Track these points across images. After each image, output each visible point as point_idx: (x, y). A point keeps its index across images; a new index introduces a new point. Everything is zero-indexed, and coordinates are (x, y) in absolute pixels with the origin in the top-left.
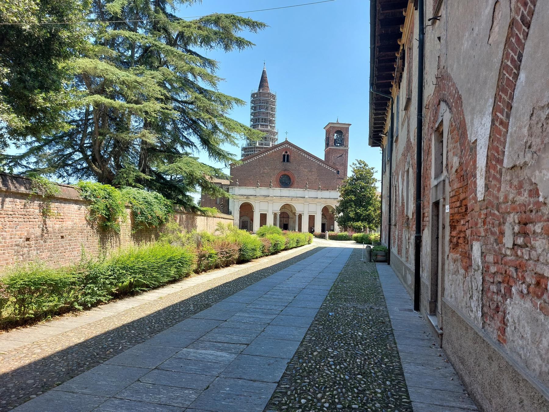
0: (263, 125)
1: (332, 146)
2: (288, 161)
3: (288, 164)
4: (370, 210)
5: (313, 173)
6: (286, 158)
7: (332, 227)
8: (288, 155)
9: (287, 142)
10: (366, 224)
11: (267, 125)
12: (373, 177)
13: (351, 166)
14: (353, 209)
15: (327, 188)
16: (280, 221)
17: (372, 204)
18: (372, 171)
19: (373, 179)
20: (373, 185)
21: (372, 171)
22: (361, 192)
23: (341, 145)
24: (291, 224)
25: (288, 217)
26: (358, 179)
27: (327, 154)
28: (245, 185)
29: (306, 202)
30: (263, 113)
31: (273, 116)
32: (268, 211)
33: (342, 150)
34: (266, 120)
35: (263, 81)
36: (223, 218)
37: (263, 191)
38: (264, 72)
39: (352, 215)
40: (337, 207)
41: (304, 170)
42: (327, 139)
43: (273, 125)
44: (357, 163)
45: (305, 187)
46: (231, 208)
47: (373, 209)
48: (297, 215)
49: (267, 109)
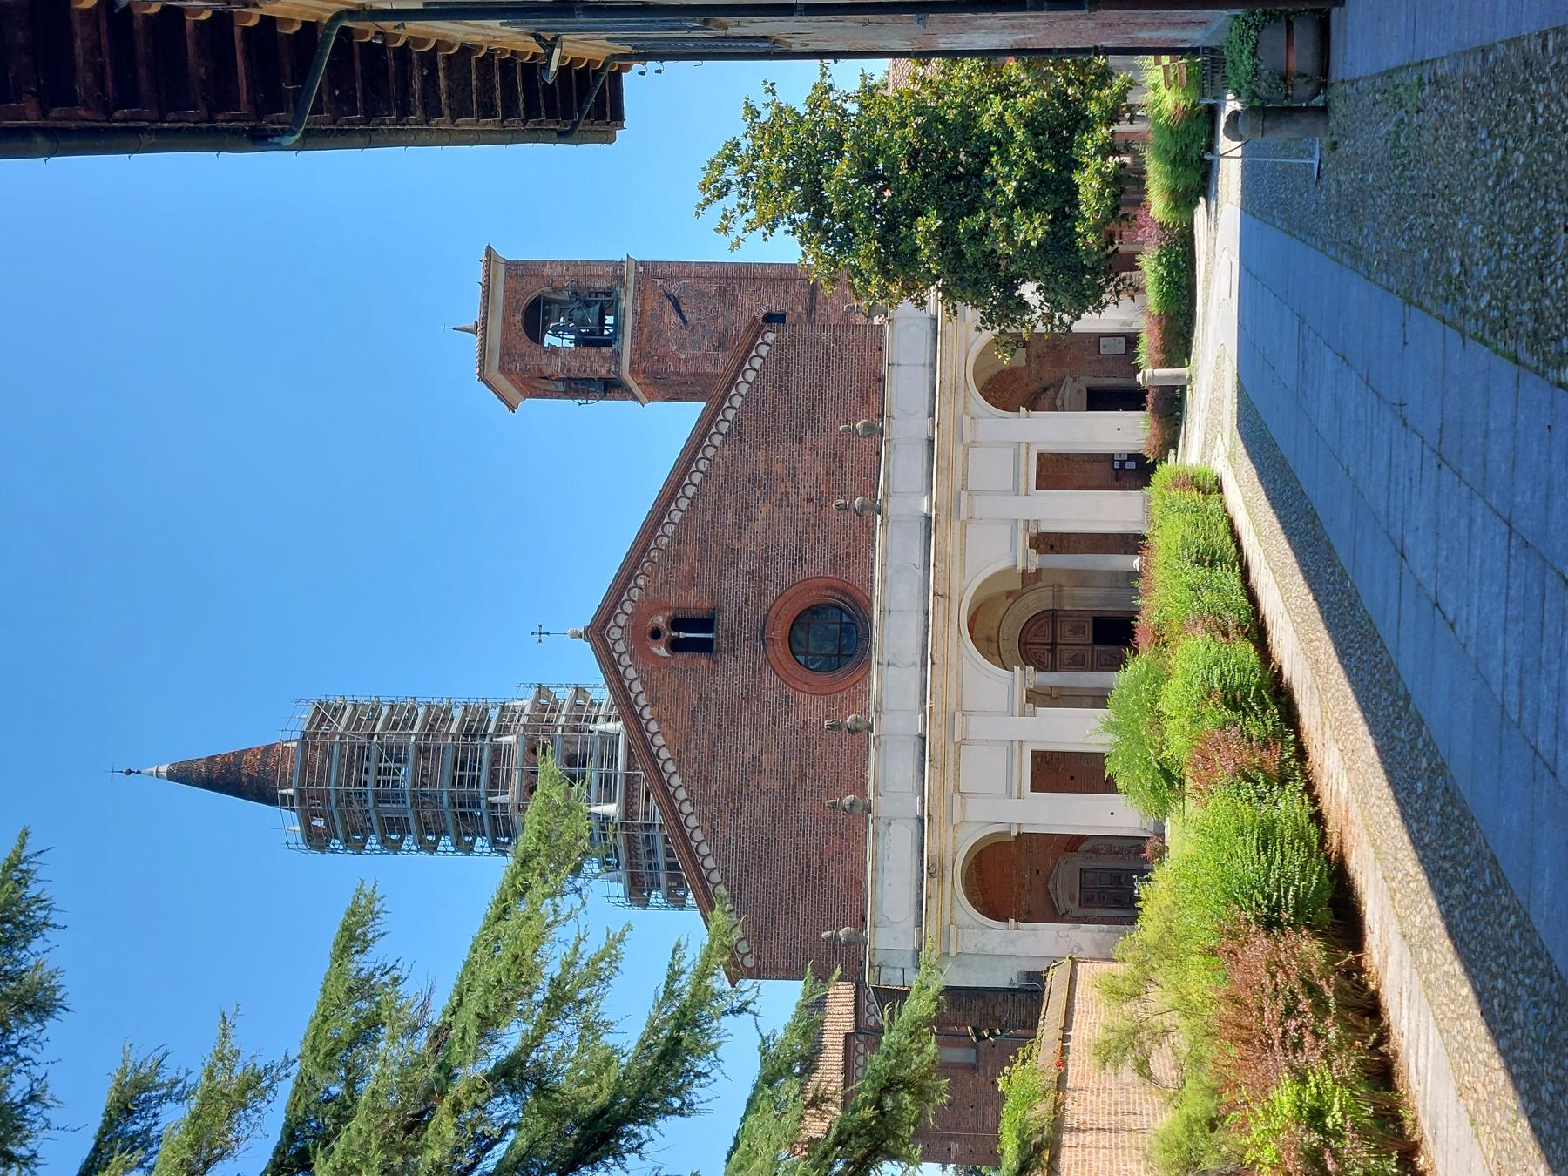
1: (617, 357)
2: (707, 624)
3: (724, 619)
4: (1000, 121)
5: (779, 469)
6: (693, 634)
7: (1107, 347)
8: (669, 623)
9: (596, 633)
11: (496, 750)
12: (803, 110)
13: (737, 244)
14: (996, 223)
15: (872, 384)
16: (1078, 664)
17: (964, 110)
19: (815, 105)
22: (889, 178)
23: (607, 302)
24: (1093, 600)
25: (1052, 616)
26: (814, 199)
30: (421, 776)
31: (437, 718)
33: (641, 296)
34: (465, 763)
36: (1067, 1025)
37: (891, 775)
38: (182, 775)
39: (1033, 229)
40: (987, 320)
41: (758, 526)
42: (578, 386)
44: (718, 206)
46: (1002, 977)
47: (997, 104)
48: (1035, 561)
49: (396, 754)
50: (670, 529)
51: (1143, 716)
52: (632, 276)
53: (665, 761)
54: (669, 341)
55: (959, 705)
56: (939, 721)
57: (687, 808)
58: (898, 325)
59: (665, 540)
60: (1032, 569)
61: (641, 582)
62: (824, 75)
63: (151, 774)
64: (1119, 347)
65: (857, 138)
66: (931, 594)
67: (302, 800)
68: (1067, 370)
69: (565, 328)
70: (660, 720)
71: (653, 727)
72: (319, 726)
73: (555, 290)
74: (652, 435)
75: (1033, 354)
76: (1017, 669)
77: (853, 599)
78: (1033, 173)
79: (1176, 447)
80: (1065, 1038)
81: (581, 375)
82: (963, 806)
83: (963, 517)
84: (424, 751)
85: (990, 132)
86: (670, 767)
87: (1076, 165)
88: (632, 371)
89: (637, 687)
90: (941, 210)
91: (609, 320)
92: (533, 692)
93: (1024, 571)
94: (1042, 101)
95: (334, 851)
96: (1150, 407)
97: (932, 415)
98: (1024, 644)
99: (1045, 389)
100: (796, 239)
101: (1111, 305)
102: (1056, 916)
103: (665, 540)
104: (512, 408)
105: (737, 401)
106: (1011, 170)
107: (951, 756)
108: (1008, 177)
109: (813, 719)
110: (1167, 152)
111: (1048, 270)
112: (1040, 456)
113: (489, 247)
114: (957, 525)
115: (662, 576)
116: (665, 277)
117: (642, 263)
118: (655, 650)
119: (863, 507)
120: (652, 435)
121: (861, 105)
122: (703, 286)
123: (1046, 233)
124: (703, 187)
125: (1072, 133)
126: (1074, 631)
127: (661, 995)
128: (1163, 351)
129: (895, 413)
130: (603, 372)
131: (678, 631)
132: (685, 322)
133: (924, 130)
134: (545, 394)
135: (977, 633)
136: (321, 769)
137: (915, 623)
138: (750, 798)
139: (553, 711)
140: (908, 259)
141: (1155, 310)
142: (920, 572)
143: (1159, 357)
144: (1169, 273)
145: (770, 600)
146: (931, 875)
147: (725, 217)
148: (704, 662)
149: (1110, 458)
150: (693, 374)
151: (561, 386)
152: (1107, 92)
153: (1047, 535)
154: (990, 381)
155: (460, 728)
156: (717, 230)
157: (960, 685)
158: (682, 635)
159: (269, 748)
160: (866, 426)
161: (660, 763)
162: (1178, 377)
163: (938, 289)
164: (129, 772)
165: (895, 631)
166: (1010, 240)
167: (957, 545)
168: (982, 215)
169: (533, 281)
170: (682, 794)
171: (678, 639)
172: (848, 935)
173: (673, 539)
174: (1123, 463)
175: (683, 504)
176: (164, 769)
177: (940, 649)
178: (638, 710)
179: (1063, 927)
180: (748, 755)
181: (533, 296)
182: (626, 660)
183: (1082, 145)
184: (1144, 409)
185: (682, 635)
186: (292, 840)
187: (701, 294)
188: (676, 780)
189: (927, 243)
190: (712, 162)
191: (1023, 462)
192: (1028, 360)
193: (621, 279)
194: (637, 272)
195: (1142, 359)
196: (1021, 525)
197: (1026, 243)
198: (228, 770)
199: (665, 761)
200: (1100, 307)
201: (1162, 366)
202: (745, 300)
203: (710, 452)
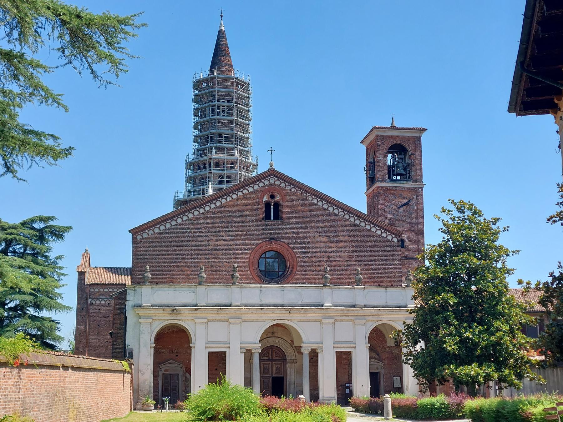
0: (223, 149)
1: (384, 181)
3: (279, 224)
4: (498, 330)
5: (341, 244)
6: (273, 211)
7: (397, 380)
8: (279, 203)
10: (491, 370)
11: (233, 149)
12: (497, 243)
13: (437, 217)
14: (452, 328)
15: (378, 280)
16: (263, 371)
17: (502, 314)
18: (494, 227)
19: (500, 248)
20: (499, 265)
21: (494, 227)
22: (469, 283)
23: (406, 177)
24: (291, 378)
25: (283, 359)
26: (460, 249)
27: (373, 201)
28: (171, 280)
29: (326, 316)
30: (222, 122)
31: (244, 128)
32: (228, 344)
33: (409, 190)
34: (228, 138)
35: (220, 55)
36: (74, 368)
37: (216, 293)
38: (221, 35)
39: (451, 345)
40: (408, 327)
41: (317, 237)
42: (371, 167)
43: (247, 149)
44: (453, 208)
45: (321, 280)
46: (130, 342)
47: (506, 328)
48: (306, 351)
49: (230, 113)
50: (315, 201)
51: (231, 401)
52: (417, 186)
53: (221, 201)
54: (391, 202)
55: (245, 320)
56: (238, 312)
57: (202, 211)
58: (403, 292)
59: (310, 199)
60: (302, 350)
61: (293, 190)
62: (513, 252)
63: (221, 24)
64: (397, 385)
65: (487, 267)
66: (290, 308)
67: (212, 78)
68: (386, 363)
69: (395, 161)
70: (238, 198)
71: (234, 196)
72: (240, 84)
73: (410, 156)
74: (354, 194)
75: (392, 349)
76: (260, 345)
77: (288, 276)
78: (476, 345)
79: (355, 411)
80: (65, 368)
81: (376, 167)
82: (202, 323)
83: (324, 320)
84: (231, 123)
85: (493, 326)
86: (218, 204)
87: (480, 366)
88: (379, 187)
89: (251, 189)
90: (457, 304)
91: (399, 178)
92: (254, 163)
93: (301, 347)
94: (507, 348)
95: (194, 92)
96: (373, 399)
97: (366, 306)
98: (272, 348)
99: (378, 355)
100: (441, 242)
101: (417, 381)
102: (157, 364)
103: (310, 199)
104: (362, 142)
105: (368, 227)
106: (477, 335)
107: (223, 318)
108: (473, 334)
109: (239, 261)
110: (504, 408)
111: (433, 352)
112: (350, 353)
113: (426, 130)
114: (319, 318)
115: (295, 198)
116: (417, 199)
117: (422, 190)
118: (266, 196)
119: (326, 278)
120: (354, 194)
121: (501, 268)
122: (414, 214)
123: (450, 351)
124: (462, 202)
125: (493, 362)
126: (278, 369)
127: (26, 128)
128: (399, 406)
129: (366, 291)
130: (378, 176)
131: (274, 206)
132: (399, 208)
133: (492, 296)
134: (368, 155)
135: (275, 328)
136: (224, 85)
137: (280, 301)
138: (206, 236)
139: (247, 170)
140: (435, 291)
141: (419, 402)
142: (300, 303)
143: (396, 404)
144: (436, 409)
145: (287, 242)
146: (173, 310)
147: (449, 211)
148: (261, 216)
149: (350, 382)
150: (378, 211)
151: (371, 160)
152: (514, 377)
153: (317, 356)
154: (380, 331)
155: (240, 136)
156: (443, 208)
157: (253, 320)
158: (272, 207)
159: (231, 66)
160: (360, 278)
161: (220, 199)
162: (388, 413)
163: (421, 305)
164: (222, 16)
165: (273, 293)
166: (445, 335)
167: (312, 318)
168: (456, 323)
169: (413, 148)
170: (207, 208)
171: (270, 205)
172: (148, 276)
173: (311, 202)
174: (348, 388)
175: (325, 206)
176: (223, 28)
177: (267, 312)
178: (241, 190)
179: (152, 367)
180: (224, 235)
181: (407, 148)
182: (261, 185)
183: (489, 366)
184: (371, 397)
185: (272, 207)
186: (197, 75)
187: (411, 214)
188: (213, 206)
189: (443, 299)
190: (472, 205)
191: (347, 345)
192: (390, 347)
193: (416, 182)
194: (419, 188)
195: (393, 395)
196: (321, 345)
197: (445, 343)
198: (223, 52)
199: (221, 201)
200: (417, 376)
201: (392, 405)
202: (409, 232)
203: (347, 216)
